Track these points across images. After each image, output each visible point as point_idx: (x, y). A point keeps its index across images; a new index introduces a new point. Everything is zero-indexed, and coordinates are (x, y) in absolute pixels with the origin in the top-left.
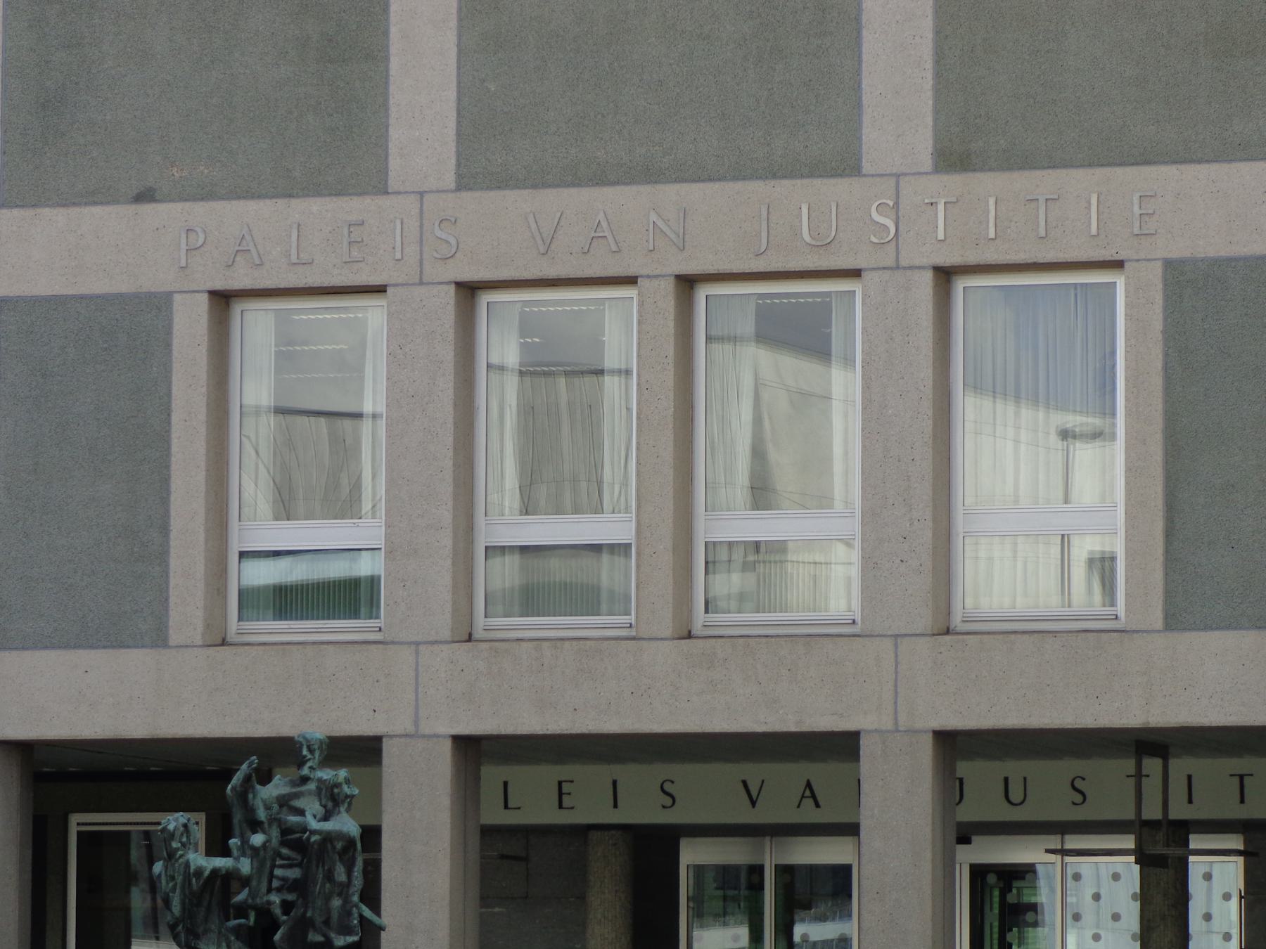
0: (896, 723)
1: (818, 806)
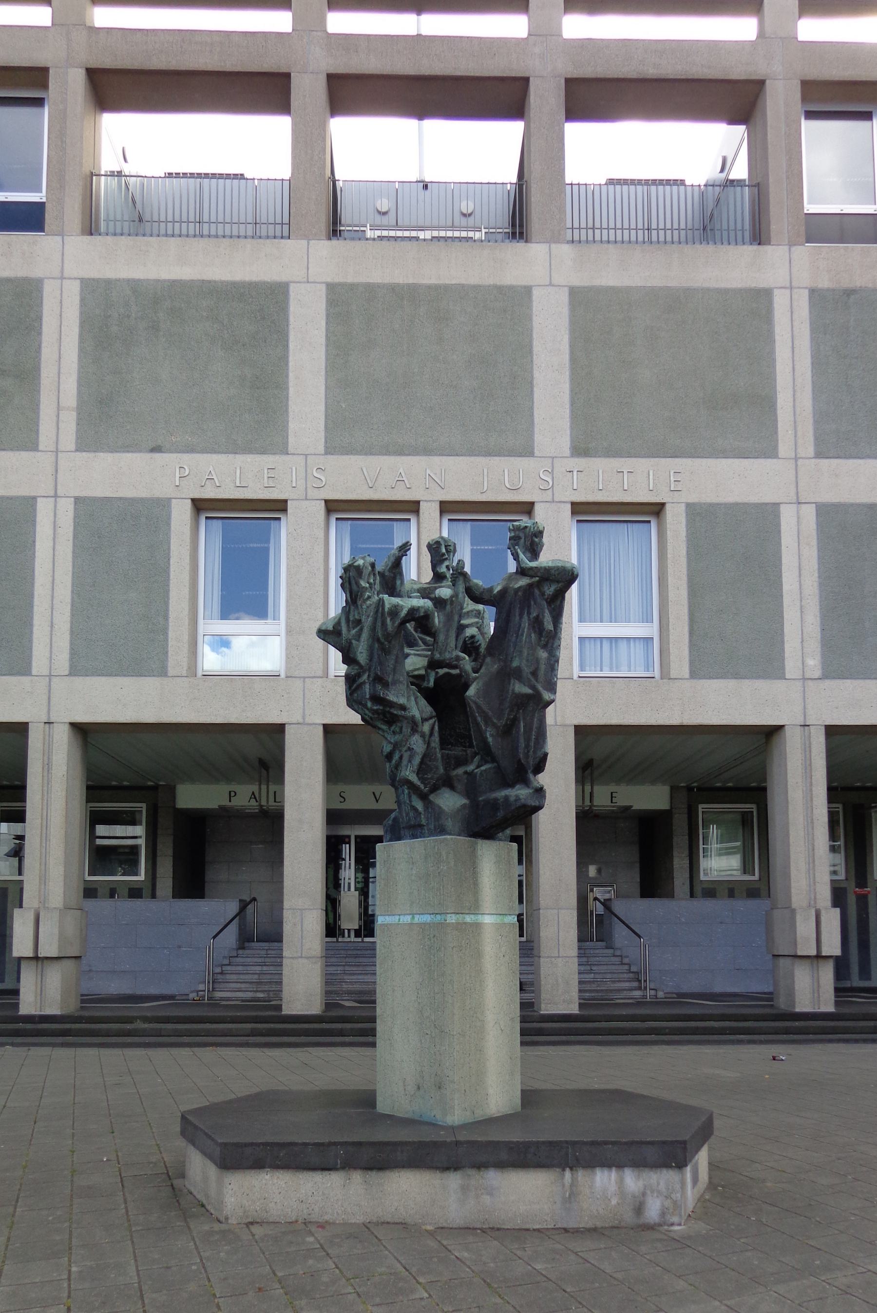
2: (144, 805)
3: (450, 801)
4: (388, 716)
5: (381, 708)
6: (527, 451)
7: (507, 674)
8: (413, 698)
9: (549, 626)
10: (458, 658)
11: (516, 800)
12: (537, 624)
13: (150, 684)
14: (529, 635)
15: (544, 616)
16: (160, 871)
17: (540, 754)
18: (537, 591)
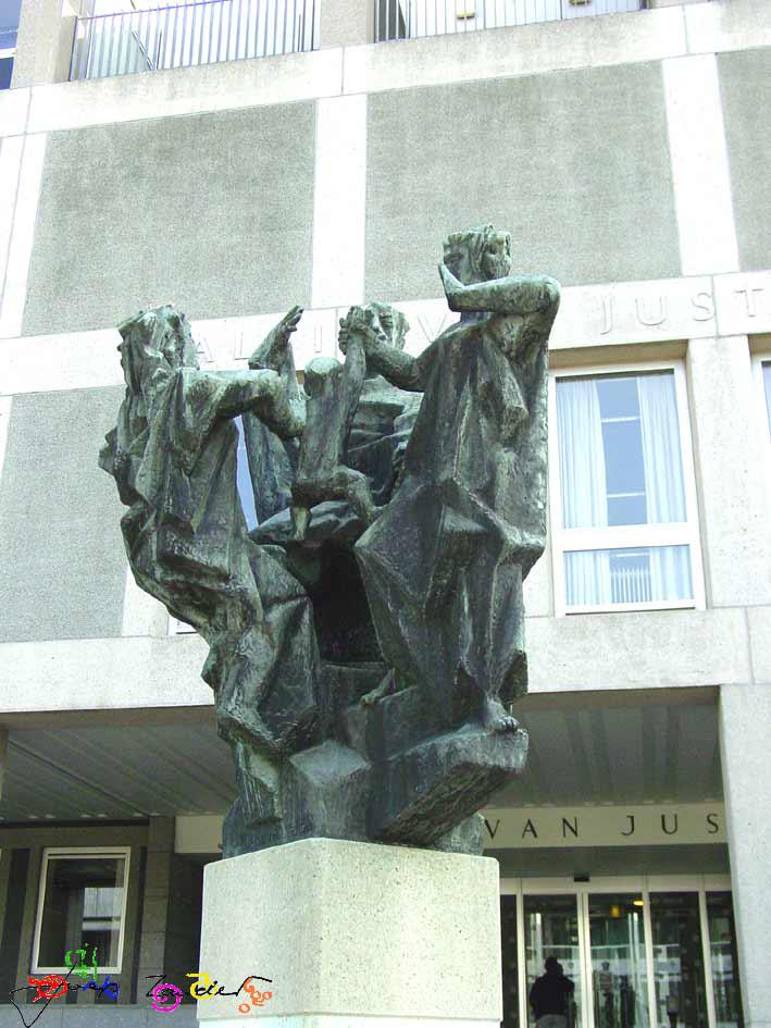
0: (753, 677)
1: (536, 836)
2: (127, 850)
3: (329, 768)
4: (199, 594)
5: (181, 578)
6: (672, 270)
7: (440, 496)
8: (245, 558)
9: (513, 397)
10: (343, 480)
11: (449, 755)
12: (491, 401)
13: (92, 650)
14: (474, 422)
15: (502, 384)
16: (145, 955)
17: (506, 655)
18: (487, 339)
